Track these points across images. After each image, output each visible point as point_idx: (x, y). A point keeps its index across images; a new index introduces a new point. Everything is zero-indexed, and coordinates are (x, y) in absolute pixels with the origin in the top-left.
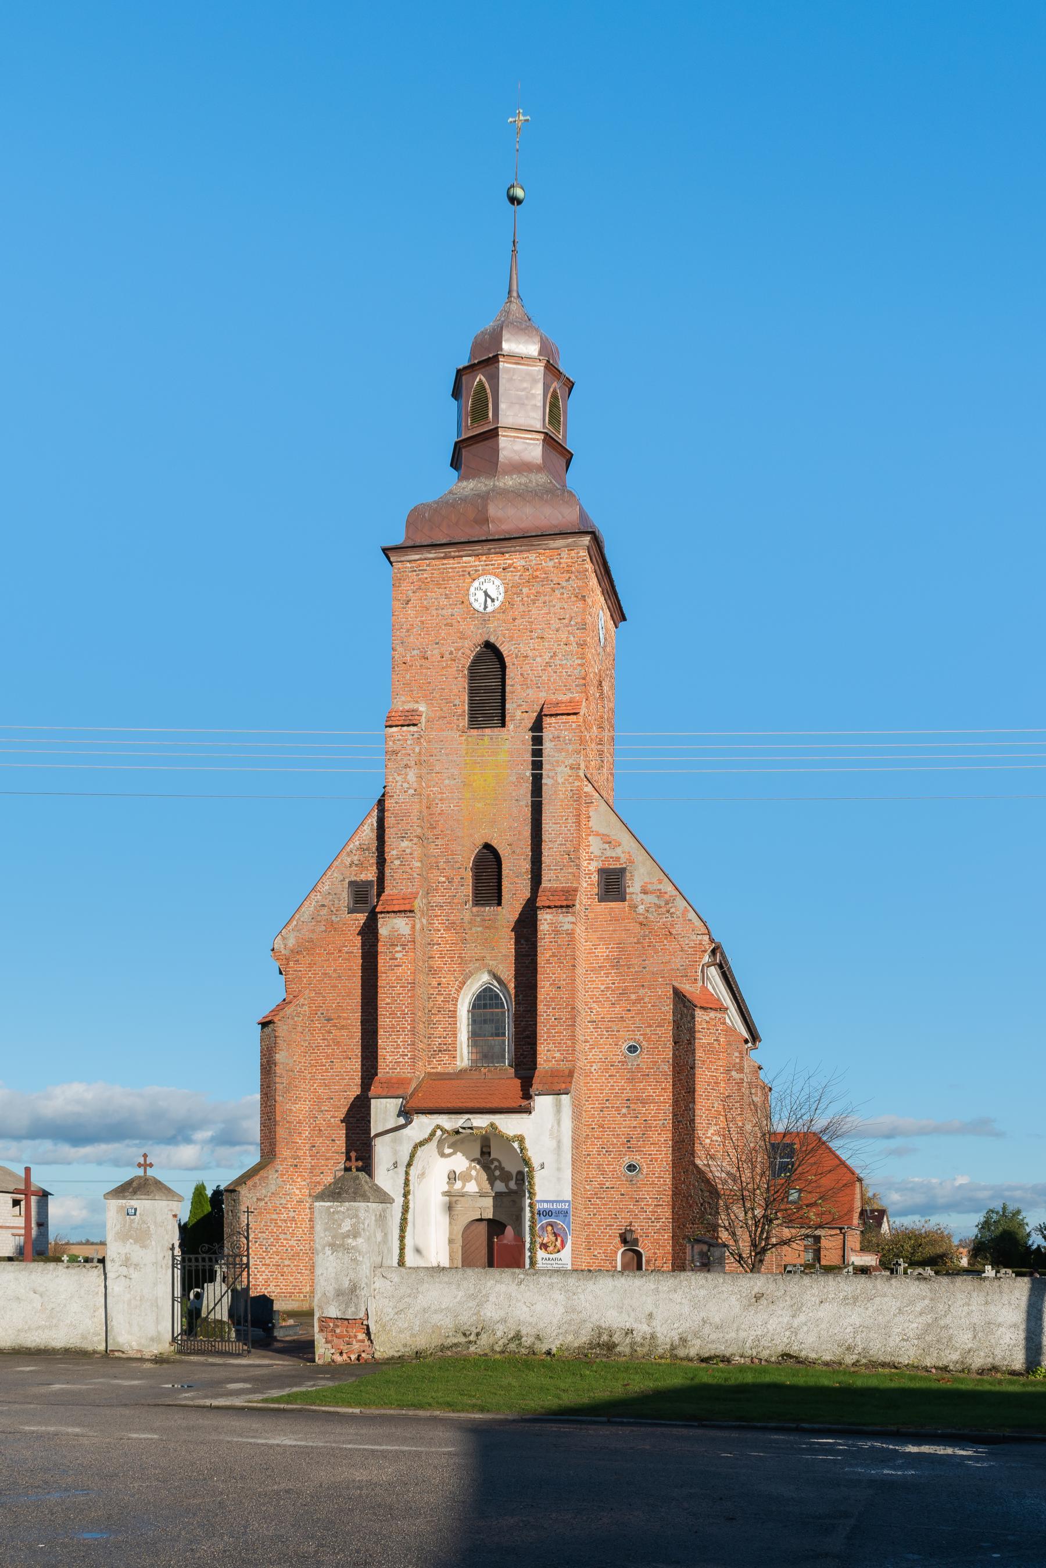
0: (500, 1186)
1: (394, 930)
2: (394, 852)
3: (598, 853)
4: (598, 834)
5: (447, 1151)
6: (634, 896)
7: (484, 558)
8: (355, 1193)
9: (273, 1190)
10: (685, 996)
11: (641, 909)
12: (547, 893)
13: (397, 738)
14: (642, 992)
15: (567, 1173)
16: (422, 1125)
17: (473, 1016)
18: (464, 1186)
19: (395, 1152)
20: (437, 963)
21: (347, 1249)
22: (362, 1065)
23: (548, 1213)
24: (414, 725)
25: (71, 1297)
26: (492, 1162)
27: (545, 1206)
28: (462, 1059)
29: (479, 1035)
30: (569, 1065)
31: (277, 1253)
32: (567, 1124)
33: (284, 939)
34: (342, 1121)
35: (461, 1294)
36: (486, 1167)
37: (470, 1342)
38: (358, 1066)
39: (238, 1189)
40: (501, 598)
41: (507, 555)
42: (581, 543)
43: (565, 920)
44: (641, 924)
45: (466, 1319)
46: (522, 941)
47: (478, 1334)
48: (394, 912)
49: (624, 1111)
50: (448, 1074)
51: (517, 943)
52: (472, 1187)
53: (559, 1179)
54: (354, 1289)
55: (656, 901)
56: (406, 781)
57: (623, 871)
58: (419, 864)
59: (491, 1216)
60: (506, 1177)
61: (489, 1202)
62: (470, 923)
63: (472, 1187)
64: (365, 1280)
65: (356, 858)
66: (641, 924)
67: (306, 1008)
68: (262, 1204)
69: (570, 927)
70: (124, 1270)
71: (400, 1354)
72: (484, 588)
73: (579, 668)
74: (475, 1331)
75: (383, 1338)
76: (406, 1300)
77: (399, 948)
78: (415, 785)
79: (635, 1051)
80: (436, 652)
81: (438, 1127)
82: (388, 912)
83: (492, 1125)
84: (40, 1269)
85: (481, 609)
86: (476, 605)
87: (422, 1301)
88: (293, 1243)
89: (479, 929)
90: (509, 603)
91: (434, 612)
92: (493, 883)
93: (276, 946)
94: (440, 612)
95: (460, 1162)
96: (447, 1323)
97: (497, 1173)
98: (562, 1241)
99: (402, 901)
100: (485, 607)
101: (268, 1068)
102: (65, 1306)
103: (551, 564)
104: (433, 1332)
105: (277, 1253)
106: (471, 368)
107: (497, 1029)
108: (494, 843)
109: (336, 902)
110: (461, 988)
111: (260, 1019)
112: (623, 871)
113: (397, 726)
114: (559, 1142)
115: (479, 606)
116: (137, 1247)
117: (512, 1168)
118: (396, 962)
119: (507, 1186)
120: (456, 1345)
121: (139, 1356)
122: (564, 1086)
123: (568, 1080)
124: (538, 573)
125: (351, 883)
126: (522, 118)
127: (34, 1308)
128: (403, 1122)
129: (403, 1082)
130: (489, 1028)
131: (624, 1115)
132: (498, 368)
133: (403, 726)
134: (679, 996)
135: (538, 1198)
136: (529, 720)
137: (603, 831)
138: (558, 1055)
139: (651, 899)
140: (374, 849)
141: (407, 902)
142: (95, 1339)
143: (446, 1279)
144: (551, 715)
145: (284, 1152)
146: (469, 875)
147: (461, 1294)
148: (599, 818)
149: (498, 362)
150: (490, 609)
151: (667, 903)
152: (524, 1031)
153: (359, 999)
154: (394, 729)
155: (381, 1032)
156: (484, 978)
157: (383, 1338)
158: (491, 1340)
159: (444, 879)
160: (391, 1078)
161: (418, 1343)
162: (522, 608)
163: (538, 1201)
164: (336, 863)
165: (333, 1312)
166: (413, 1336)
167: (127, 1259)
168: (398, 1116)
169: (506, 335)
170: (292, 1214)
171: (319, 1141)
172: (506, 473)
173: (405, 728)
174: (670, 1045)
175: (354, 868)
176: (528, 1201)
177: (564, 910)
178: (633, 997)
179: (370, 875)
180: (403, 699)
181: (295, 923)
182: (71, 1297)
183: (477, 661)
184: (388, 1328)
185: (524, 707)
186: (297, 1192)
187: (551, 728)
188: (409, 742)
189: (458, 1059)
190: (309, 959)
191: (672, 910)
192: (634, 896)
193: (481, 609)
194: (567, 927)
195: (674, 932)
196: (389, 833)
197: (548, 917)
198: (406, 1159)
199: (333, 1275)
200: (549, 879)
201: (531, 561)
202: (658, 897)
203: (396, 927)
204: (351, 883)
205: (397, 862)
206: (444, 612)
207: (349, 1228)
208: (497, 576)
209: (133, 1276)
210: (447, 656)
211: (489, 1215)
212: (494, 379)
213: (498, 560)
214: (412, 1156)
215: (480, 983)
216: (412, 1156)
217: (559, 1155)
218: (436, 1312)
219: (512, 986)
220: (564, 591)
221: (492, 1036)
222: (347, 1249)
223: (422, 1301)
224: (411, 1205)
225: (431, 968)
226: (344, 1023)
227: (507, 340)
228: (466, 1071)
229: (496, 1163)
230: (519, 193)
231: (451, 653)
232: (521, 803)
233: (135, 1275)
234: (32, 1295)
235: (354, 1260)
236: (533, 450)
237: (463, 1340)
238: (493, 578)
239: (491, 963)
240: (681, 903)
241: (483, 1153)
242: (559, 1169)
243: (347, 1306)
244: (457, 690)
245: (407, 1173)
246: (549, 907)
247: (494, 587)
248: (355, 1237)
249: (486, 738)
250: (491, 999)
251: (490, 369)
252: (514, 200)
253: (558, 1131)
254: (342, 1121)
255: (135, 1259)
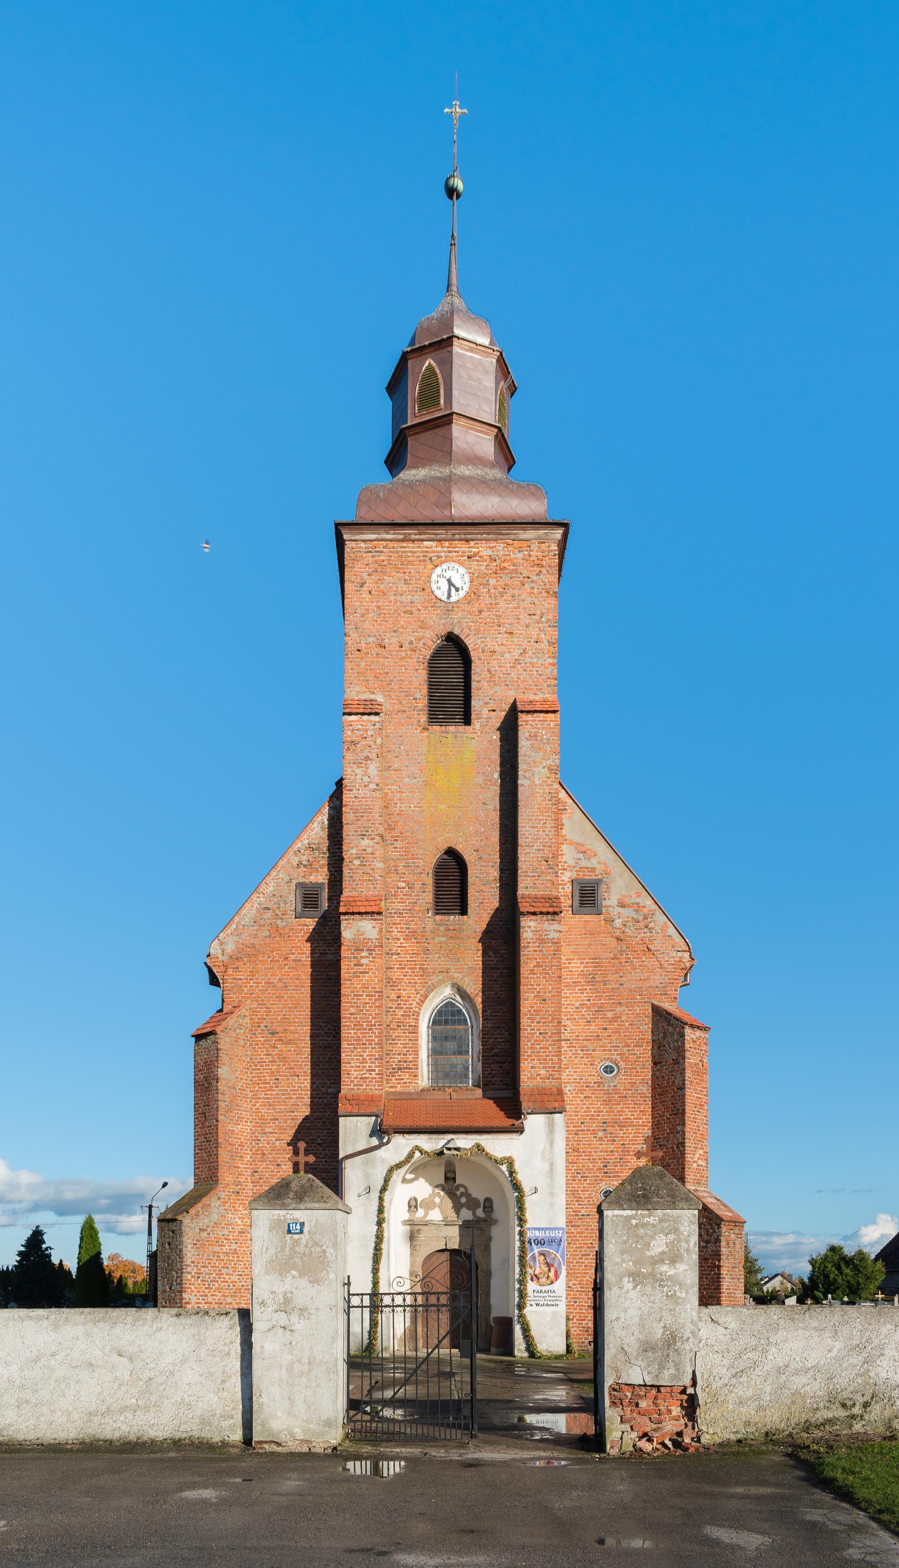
0: (467, 1214)
1: (359, 933)
2: (354, 851)
3: (571, 862)
4: (571, 843)
5: (410, 1176)
6: (610, 909)
7: (447, 544)
8: (672, 1196)
9: (215, 1220)
10: (670, 1014)
11: (618, 923)
12: (528, 900)
13: (356, 727)
14: (619, 1009)
15: (561, 1199)
16: (400, 1146)
17: (433, 1032)
18: (426, 1214)
19: (367, 1176)
20: (396, 974)
21: (660, 1281)
22: (312, 1083)
23: (540, 1242)
24: (377, 714)
25: (184, 1361)
26: (457, 1188)
27: (537, 1233)
28: (422, 1081)
29: (441, 1053)
30: (555, 1083)
31: (219, 1289)
32: (560, 1146)
33: (222, 943)
34: (289, 1144)
35: (838, 1345)
36: (451, 1194)
37: (853, 1417)
38: (307, 1083)
39: (179, 1218)
40: (466, 588)
41: (472, 543)
42: (552, 536)
43: (551, 928)
44: (618, 939)
45: (846, 1381)
46: (490, 954)
47: (866, 1405)
48: (360, 913)
49: (600, 1134)
50: (409, 1093)
51: (485, 954)
52: (435, 1215)
53: (552, 1205)
54: (671, 1340)
55: (635, 916)
56: (366, 774)
57: (598, 882)
58: (381, 865)
59: (456, 1246)
60: (472, 1204)
61: (454, 1232)
62: (432, 932)
63: (435, 1215)
64: (689, 1327)
65: (304, 858)
66: (618, 939)
67: (247, 1020)
68: (204, 1234)
69: (556, 935)
70: (282, 1319)
71: (739, 1436)
72: (448, 575)
73: (551, 668)
74: (861, 1400)
75: (715, 1412)
76: (750, 1355)
77: (365, 954)
78: (377, 780)
79: (612, 1072)
80: (394, 640)
81: (417, 1148)
82: (353, 913)
83: (478, 1146)
84: (130, 1319)
85: (444, 598)
86: (438, 594)
87: (775, 1357)
88: (235, 1278)
89: (443, 939)
90: (474, 594)
91: (392, 598)
92: (456, 891)
93: (212, 952)
94: (398, 598)
95: (422, 1189)
96: (813, 1388)
97: (463, 1200)
98: (556, 1272)
99: (366, 903)
100: (449, 596)
101: (205, 1085)
102: (172, 1373)
103: (520, 555)
104: (793, 1403)
105: (219, 1289)
106: (420, 351)
107: (459, 1046)
108: (459, 848)
109: (282, 905)
110: (423, 1002)
111: (193, 1031)
112: (598, 882)
113: (357, 714)
114: (552, 1165)
115: (442, 594)
116: (304, 1282)
117: (479, 1194)
118: (362, 969)
119: (474, 1214)
120: (829, 1421)
121: (305, 1449)
122: (556, 1104)
123: (559, 1098)
124: (506, 565)
125: (299, 885)
126: (458, 110)
127: (116, 1378)
128: (377, 1143)
129: (371, 1099)
130: (451, 1045)
131: (601, 1139)
132: (451, 353)
133: (363, 714)
134: (660, 1015)
135: (528, 1225)
136: (498, 718)
137: (577, 839)
138: (543, 1072)
139: (628, 913)
140: (325, 850)
141: (372, 903)
142: (226, 1424)
143: (815, 1324)
144: (528, 712)
145: (226, 1177)
146: (430, 880)
147: (838, 1345)
148: (575, 826)
149: (452, 345)
150: (454, 598)
151: (645, 918)
152: (493, 1049)
153: (308, 1012)
154: (353, 718)
155: (344, 1045)
156: (446, 992)
157: (715, 1412)
158: (887, 1413)
159: (403, 885)
160: (358, 1096)
161: (768, 1420)
162: (488, 600)
163: (529, 1229)
164: (281, 863)
165: (636, 1375)
166: (760, 1408)
167: (287, 1301)
168: (371, 1136)
169: (457, 321)
170: (234, 1246)
171: (262, 1166)
172: (460, 463)
173: (365, 717)
174: (649, 1065)
175: (302, 869)
176: (518, 1229)
177: (549, 917)
178: (610, 1015)
179: (321, 877)
180: (358, 688)
181: (234, 926)
182: (184, 1361)
183: (437, 655)
184: (721, 1398)
185: (492, 705)
186: (239, 1222)
187: (527, 725)
188: (370, 733)
189: (420, 1077)
190: (249, 967)
191: (651, 925)
192: (610, 909)
193: (444, 598)
194: (552, 935)
195: (652, 947)
196: (349, 832)
197: (532, 924)
198: (380, 1183)
199: (636, 1320)
200: (526, 887)
201: (498, 551)
202: (637, 911)
203: (362, 930)
204: (299, 885)
205: (357, 862)
206: (403, 598)
207: (664, 1248)
208: (462, 564)
209: (297, 1327)
210: (406, 645)
211: (454, 1245)
212: (447, 364)
213: (462, 547)
214: (387, 1180)
215: (442, 997)
216: (387, 1180)
217: (552, 1179)
218: (797, 1373)
219: (479, 1000)
220: (534, 585)
221: (454, 1054)
222: (660, 1281)
223: (775, 1357)
224: (385, 1234)
225: (389, 980)
226: (291, 1037)
227: (458, 326)
228: (428, 1090)
229: (462, 1190)
230: (459, 184)
231: (411, 643)
232: (488, 807)
233: (300, 1325)
234: (115, 1358)
235: (672, 1297)
236: (486, 446)
237: (842, 1413)
238: (457, 566)
239: (456, 975)
240: (660, 918)
241: (447, 1179)
242: (552, 1194)
243: (661, 1368)
244: (416, 682)
245: (381, 1199)
246: (534, 914)
247: (459, 575)
248: (673, 1262)
249: (450, 736)
250: (453, 1015)
251: (442, 353)
252: (451, 192)
253: (551, 1153)
254: (289, 1144)
255: (300, 1300)
